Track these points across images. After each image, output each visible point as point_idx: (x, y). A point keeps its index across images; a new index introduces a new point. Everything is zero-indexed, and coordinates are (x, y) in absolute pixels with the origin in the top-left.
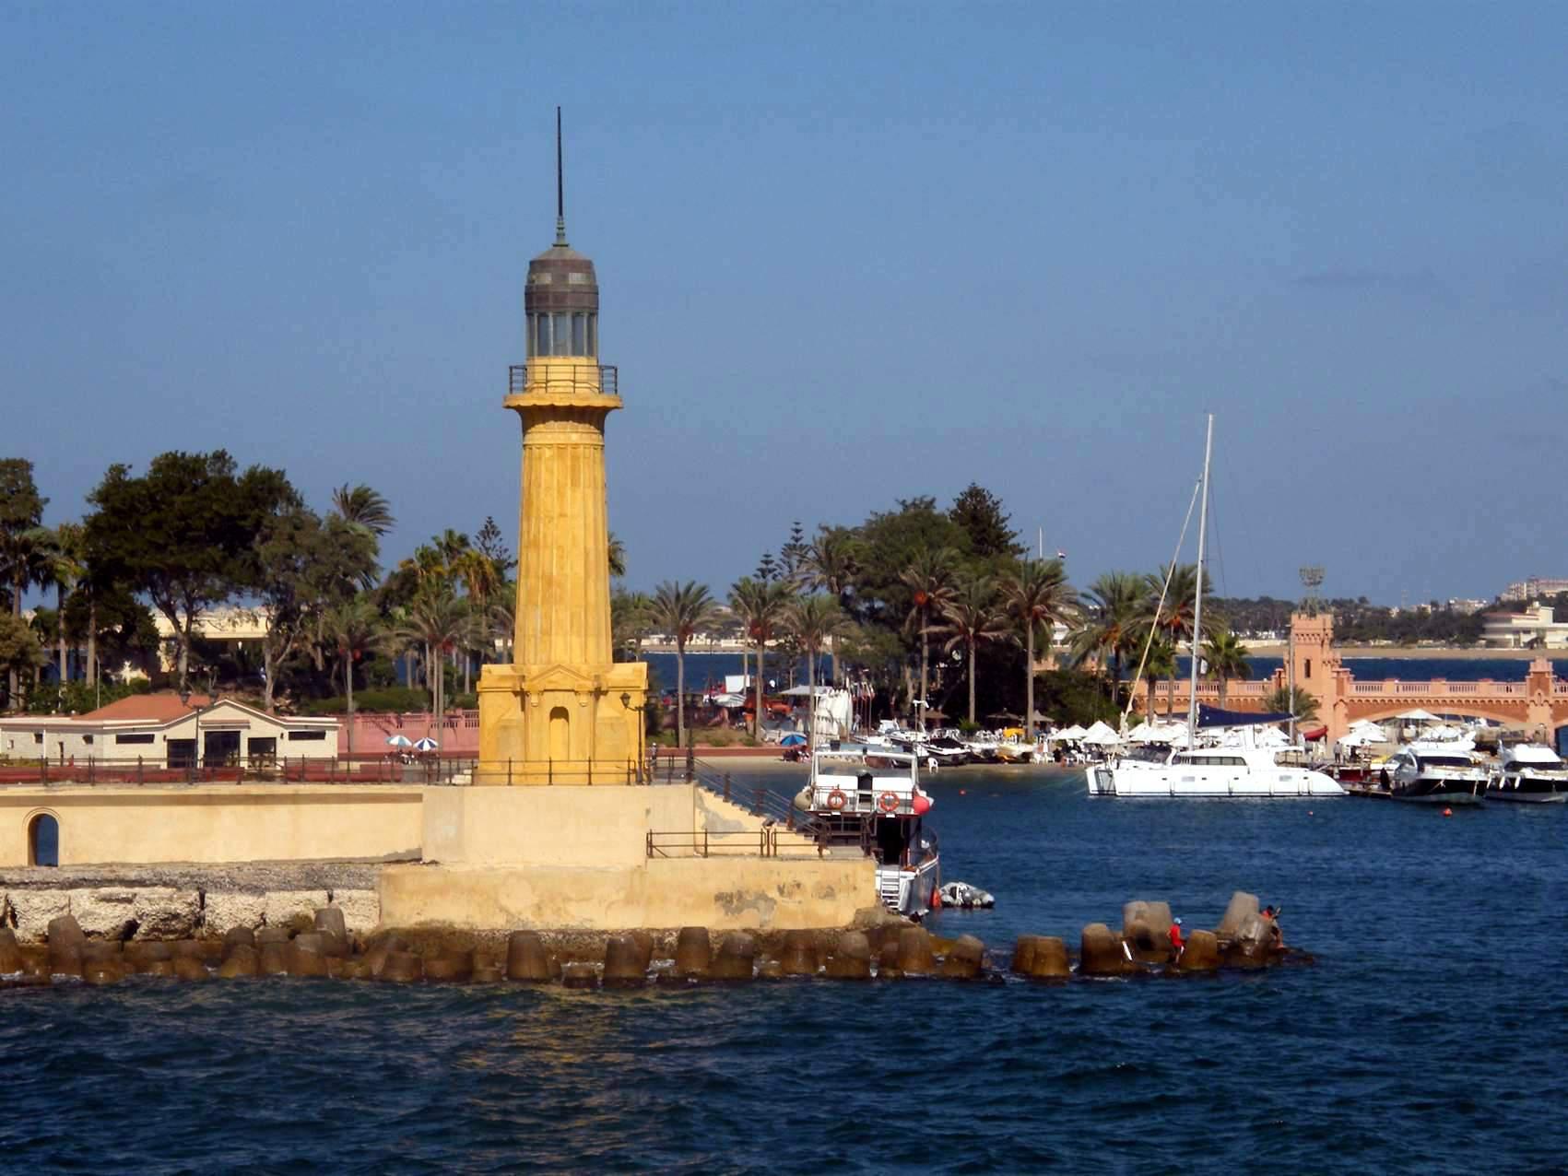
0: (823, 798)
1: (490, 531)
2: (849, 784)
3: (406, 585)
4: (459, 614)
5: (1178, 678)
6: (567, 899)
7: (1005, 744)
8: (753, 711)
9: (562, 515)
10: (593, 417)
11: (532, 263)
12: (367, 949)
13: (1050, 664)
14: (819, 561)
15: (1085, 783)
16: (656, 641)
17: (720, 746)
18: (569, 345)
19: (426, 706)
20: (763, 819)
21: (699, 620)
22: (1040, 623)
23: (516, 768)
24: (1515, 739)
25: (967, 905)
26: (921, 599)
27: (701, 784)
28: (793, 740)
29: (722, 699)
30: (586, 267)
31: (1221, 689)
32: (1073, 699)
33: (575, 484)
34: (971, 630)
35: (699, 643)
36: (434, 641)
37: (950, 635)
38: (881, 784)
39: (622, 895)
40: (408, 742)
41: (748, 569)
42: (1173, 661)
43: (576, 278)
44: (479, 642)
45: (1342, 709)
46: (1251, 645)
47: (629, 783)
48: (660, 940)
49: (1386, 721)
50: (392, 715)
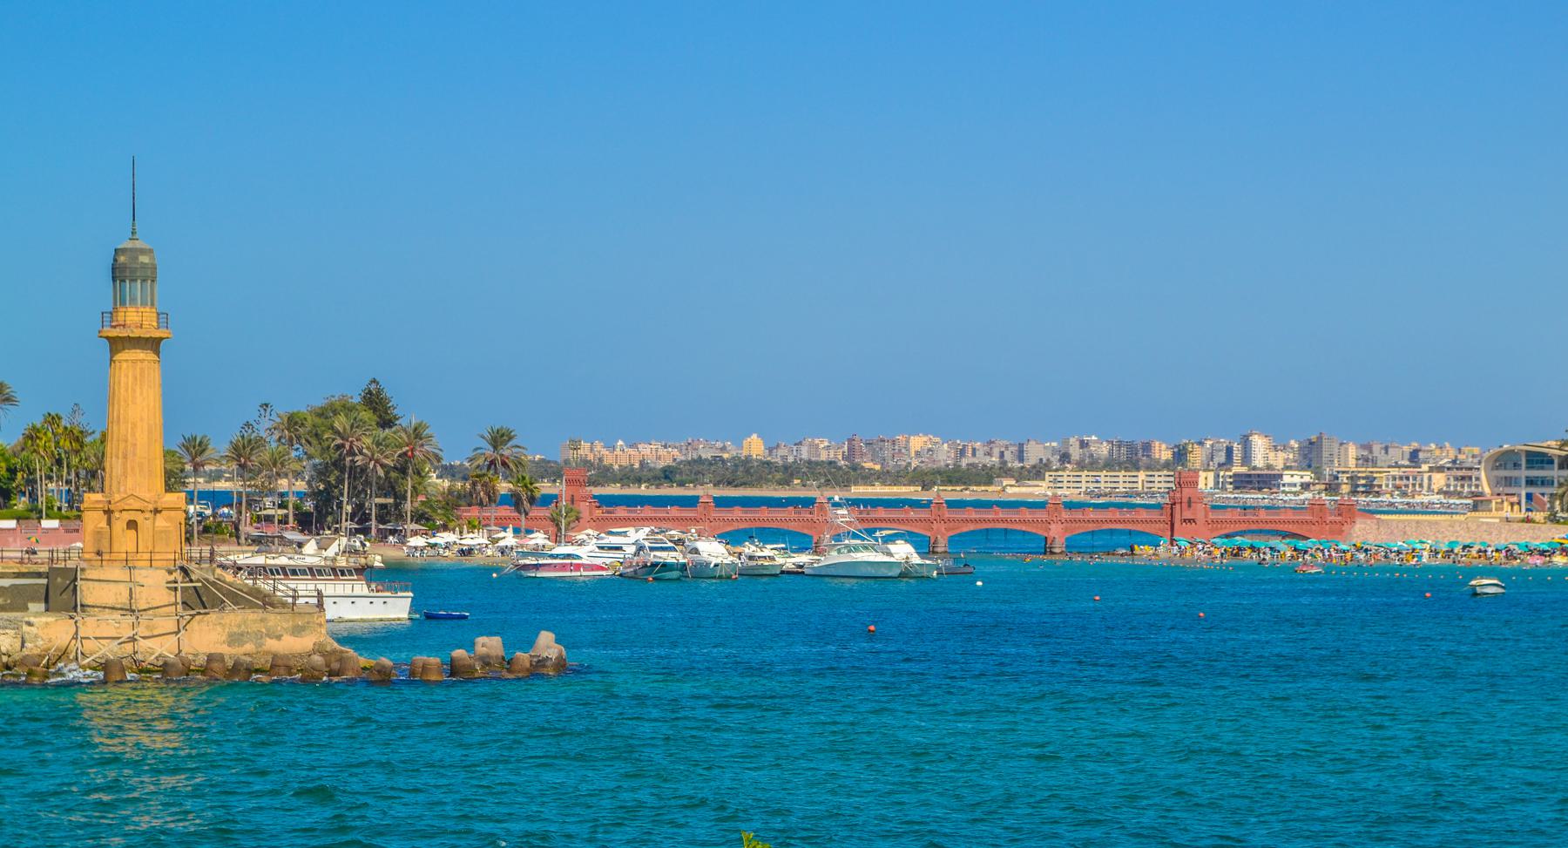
10: (153, 344)
43: (144, 259)
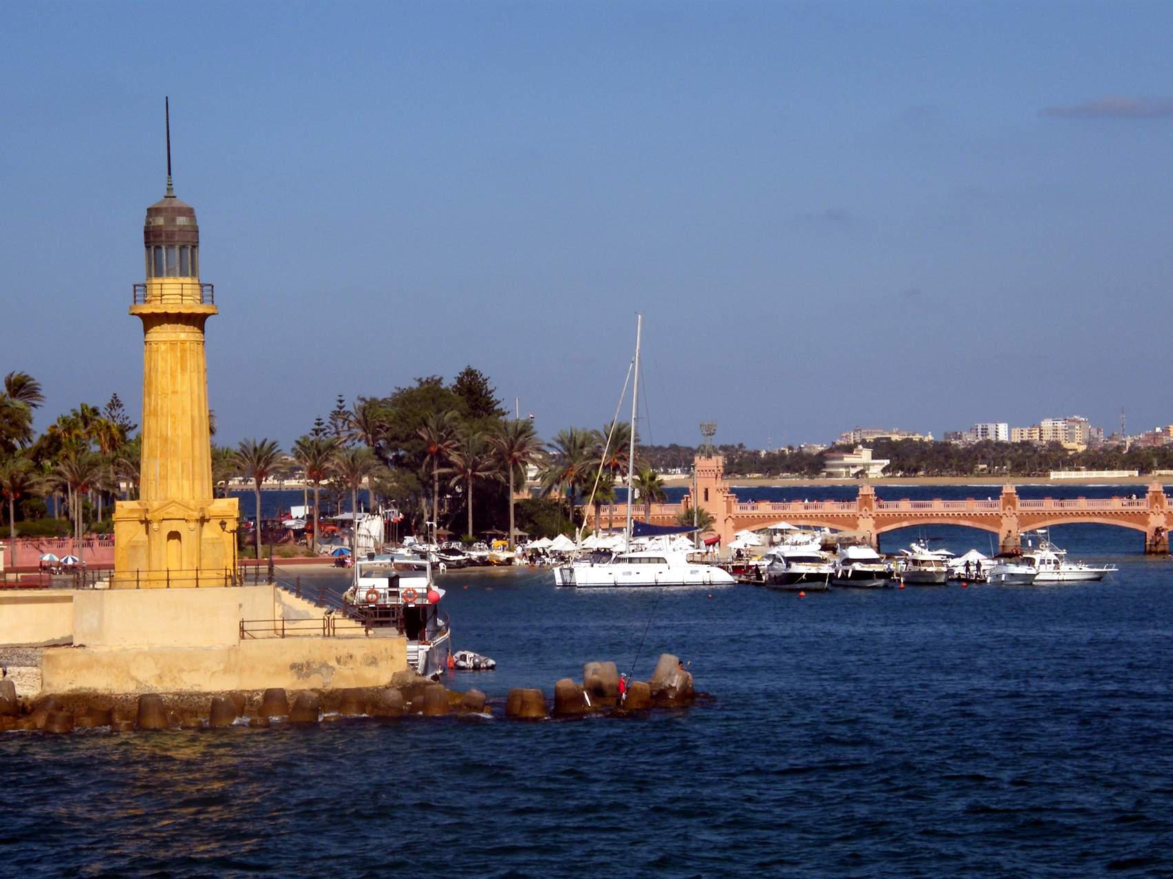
0: (362, 595)
1: (115, 404)
2: (382, 584)
3: (53, 444)
4: (93, 465)
5: (616, 502)
6: (182, 670)
7: (494, 552)
8: (312, 531)
9: (174, 392)
10: (196, 321)
11: (149, 210)
12: (33, 710)
13: (525, 495)
14: (358, 421)
15: (553, 577)
16: (237, 482)
17: (288, 557)
18: (178, 269)
19: (69, 532)
20: (325, 610)
21: (271, 466)
22: (517, 466)
23: (142, 576)
24: (851, 542)
25: (476, 668)
26: (433, 449)
27: (278, 586)
28: (341, 552)
29: (288, 523)
30: (189, 212)
31: (647, 510)
32: (542, 519)
33: (183, 369)
34: (470, 471)
35: (270, 482)
36: (75, 485)
37: (453, 475)
38: (405, 583)
39: (222, 666)
40: (56, 559)
41: (305, 429)
42: (613, 491)
43: (181, 221)
44: (109, 485)
45: (731, 523)
46: (665, 478)
47: (226, 585)
48: (250, 699)
49: (759, 531)
50: (43, 539)
